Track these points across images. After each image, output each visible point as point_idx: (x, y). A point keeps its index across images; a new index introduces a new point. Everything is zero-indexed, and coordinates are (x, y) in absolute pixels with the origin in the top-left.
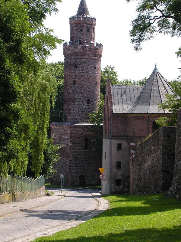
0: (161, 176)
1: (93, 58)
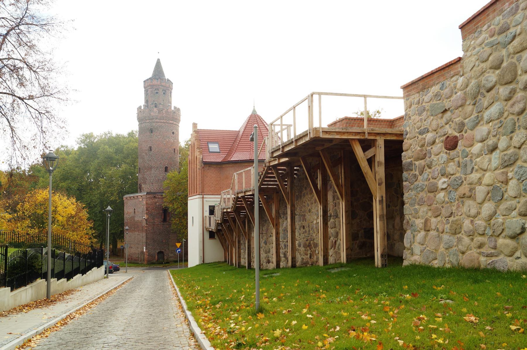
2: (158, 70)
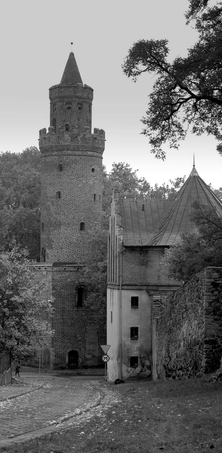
2: (72, 69)
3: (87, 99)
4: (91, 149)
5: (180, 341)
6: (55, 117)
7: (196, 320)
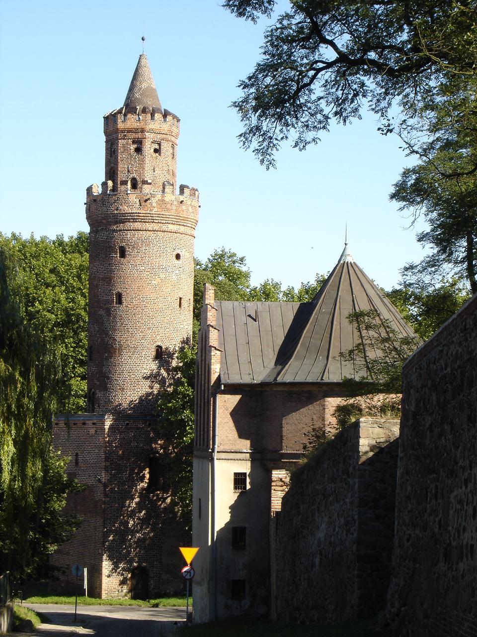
0: (356, 572)
1: (171, 227)
3: (167, 134)
4: (174, 220)
5: (313, 556)
6: (113, 165)
7: (342, 517)
